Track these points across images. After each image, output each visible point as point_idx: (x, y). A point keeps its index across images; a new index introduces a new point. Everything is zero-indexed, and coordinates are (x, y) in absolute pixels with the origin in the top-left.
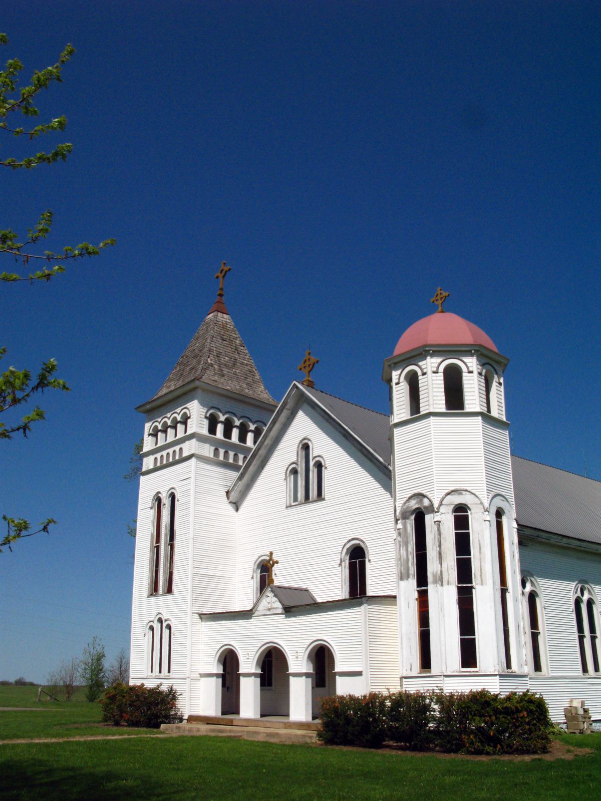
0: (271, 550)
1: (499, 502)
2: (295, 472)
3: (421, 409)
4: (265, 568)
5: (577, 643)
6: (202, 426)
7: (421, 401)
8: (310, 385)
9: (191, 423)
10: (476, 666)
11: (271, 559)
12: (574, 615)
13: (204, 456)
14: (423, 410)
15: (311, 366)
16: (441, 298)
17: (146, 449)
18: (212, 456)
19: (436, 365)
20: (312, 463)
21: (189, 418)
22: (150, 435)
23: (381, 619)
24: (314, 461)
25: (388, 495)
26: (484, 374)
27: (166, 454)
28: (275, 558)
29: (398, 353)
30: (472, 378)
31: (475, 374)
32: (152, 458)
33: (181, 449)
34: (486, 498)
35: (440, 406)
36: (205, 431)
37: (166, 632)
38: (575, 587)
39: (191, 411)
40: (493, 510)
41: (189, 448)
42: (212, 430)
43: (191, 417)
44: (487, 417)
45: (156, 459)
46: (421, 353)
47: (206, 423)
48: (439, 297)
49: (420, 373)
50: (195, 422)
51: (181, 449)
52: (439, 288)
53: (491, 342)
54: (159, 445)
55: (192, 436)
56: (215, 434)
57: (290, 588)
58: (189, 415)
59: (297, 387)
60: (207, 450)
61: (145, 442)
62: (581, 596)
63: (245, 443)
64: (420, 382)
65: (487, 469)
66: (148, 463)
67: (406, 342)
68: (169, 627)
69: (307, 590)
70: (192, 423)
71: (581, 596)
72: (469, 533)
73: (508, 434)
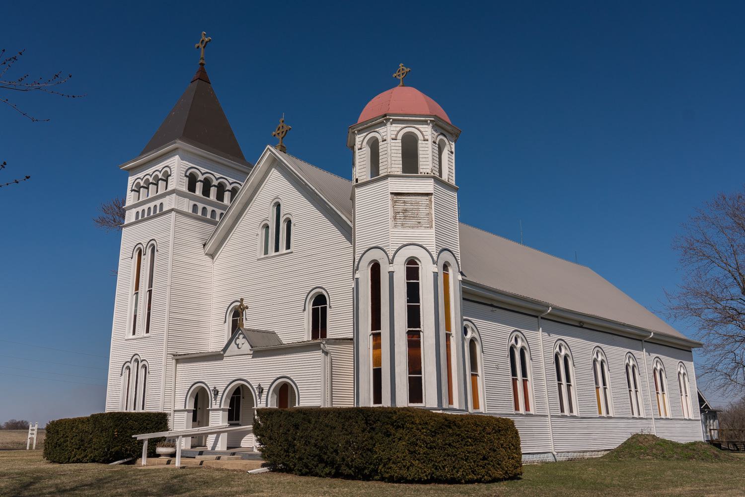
0: (242, 297)
1: (446, 256)
2: (267, 227)
3: (380, 172)
4: (238, 313)
5: (512, 404)
6: (182, 183)
7: (380, 165)
8: (283, 150)
9: (171, 181)
10: (421, 402)
11: (242, 305)
12: (509, 360)
13: (183, 211)
14: (382, 173)
15: (284, 133)
16: (403, 74)
17: (128, 204)
18: (190, 211)
19: (396, 133)
20: (282, 220)
21: (170, 175)
22: (132, 191)
23: (341, 352)
24: (285, 217)
25: (349, 244)
26: (437, 143)
27: (142, 210)
28: (245, 303)
29: (360, 122)
30: (427, 146)
31: (430, 142)
32: (134, 211)
33: (161, 204)
34: (434, 250)
35: (398, 170)
36: (185, 189)
37: (142, 372)
38: (510, 335)
39: (172, 170)
40: (441, 263)
41: (169, 202)
42: (192, 188)
43: (172, 175)
44: (438, 181)
45: (138, 212)
46: (384, 119)
47: (186, 180)
48: (401, 73)
49: (380, 140)
50: (175, 180)
51: (161, 204)
52: (402, 64)
53: (446, 114)
54: (159, 193)
55: (173, 192)
56: (194, 192)
57: (258, 331)
58: (169, 173)
59: (270, 151)
60: (186, 205)
61: (127, 197)
62: (515, 344)
63: (223, 202)
64: (380, 147)
65: (437, 244)
66: (130, 216)
67: (371, 109)
68: (145, 367)
69: (274, 333)
70: (172, 180)
71: (515, 344)
72: (418, 283)
73: (456, 195)
